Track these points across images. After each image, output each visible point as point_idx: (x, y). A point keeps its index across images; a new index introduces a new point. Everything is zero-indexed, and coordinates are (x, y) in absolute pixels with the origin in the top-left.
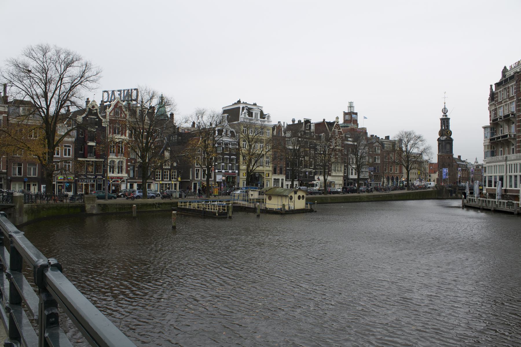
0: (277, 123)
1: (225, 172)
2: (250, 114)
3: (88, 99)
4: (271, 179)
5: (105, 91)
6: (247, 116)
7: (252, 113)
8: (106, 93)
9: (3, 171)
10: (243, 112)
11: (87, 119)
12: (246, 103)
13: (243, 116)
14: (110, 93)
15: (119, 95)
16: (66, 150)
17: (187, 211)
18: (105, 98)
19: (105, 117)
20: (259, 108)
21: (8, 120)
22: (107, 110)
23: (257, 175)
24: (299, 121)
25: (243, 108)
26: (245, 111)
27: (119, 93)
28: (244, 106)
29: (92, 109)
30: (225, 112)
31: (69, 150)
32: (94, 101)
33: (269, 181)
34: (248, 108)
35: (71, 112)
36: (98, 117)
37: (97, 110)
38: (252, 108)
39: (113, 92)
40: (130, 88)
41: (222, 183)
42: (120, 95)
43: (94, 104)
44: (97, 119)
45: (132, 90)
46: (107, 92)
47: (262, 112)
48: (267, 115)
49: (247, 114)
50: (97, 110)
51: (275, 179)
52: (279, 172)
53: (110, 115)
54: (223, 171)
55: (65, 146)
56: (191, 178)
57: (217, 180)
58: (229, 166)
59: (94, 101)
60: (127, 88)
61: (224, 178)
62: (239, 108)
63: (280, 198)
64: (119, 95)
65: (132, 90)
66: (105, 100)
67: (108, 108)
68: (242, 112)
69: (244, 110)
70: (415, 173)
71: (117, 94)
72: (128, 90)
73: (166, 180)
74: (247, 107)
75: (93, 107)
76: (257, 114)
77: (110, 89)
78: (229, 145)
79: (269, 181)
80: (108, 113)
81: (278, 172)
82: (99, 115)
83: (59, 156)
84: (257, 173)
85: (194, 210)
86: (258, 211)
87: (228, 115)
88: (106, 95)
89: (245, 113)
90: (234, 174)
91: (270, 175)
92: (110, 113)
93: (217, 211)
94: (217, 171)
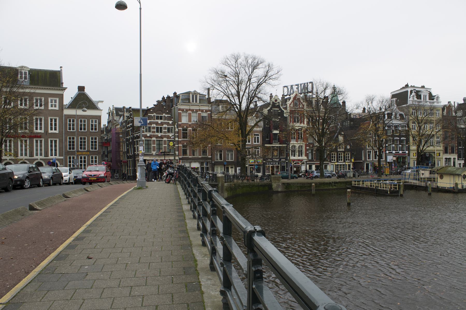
2: (419, 97)
3: (271, 94)
4: (443, 158)
5: (285, 87)
6: (416, 99)
7: (420, 96)
8: (286, 88)
10: (412, 96)
13: (411, 99)
14: (289, 87)
17: (360, 189)
18: (285, 92)
19: (286, 108)
21: (211, 116)
22: (288, 102)
23: (428, 154)
25: (411, 92)
26: (413, 94)
27: (297, 87)
28: (412, 89)
29: (275, 102)
30: (393, 96)
31: (258, 138)
32: (276, 96)
33: (440, 160)
35: (258, 107)
36: (280, 109)
37: (279, 103)
38: (420, 91)
39: (292, 86)
40: (306, 82)
41: (393, 163)
42: (298, 88)
43: (276, 98)
45: (307, 83)
46: (287, 87)
47: (430, 94)
48: (435, 96)
49: (416, 96)
50: (279, 103)
51: (446, 158)
52: (450, 151)
53: (290, 107)
54: (394, 152)
55: (255, 135)
57: (388, 161)
58: (399, 147)
59: (276, 96)
60: (304, 82)
61: (395, 159)
62: (407, 91)
63: (452, 178)
65: (307, 83)
66: (285, 94)
67: (288, 100)
68: (410, 95)
69: (413, 93)
71: (295, 88)
72: (305, 84)
73: (341, 161)
74: (415, 90)
75: (276, 100)
76: (426, 96)
77: (289, 84)
79: (440, 160)
80: (288, 105)
81: (449, 152)
82: (281, 107)
84: (427, 153)
85: (367, 189)
86: (430, 190)
87: (396, 99)
88: (286, 89)
89: (413, 96)
90: (404, 155)
91: (441, 154)
92: (290, 105)
93: (389, 189)
94: (387, 152)
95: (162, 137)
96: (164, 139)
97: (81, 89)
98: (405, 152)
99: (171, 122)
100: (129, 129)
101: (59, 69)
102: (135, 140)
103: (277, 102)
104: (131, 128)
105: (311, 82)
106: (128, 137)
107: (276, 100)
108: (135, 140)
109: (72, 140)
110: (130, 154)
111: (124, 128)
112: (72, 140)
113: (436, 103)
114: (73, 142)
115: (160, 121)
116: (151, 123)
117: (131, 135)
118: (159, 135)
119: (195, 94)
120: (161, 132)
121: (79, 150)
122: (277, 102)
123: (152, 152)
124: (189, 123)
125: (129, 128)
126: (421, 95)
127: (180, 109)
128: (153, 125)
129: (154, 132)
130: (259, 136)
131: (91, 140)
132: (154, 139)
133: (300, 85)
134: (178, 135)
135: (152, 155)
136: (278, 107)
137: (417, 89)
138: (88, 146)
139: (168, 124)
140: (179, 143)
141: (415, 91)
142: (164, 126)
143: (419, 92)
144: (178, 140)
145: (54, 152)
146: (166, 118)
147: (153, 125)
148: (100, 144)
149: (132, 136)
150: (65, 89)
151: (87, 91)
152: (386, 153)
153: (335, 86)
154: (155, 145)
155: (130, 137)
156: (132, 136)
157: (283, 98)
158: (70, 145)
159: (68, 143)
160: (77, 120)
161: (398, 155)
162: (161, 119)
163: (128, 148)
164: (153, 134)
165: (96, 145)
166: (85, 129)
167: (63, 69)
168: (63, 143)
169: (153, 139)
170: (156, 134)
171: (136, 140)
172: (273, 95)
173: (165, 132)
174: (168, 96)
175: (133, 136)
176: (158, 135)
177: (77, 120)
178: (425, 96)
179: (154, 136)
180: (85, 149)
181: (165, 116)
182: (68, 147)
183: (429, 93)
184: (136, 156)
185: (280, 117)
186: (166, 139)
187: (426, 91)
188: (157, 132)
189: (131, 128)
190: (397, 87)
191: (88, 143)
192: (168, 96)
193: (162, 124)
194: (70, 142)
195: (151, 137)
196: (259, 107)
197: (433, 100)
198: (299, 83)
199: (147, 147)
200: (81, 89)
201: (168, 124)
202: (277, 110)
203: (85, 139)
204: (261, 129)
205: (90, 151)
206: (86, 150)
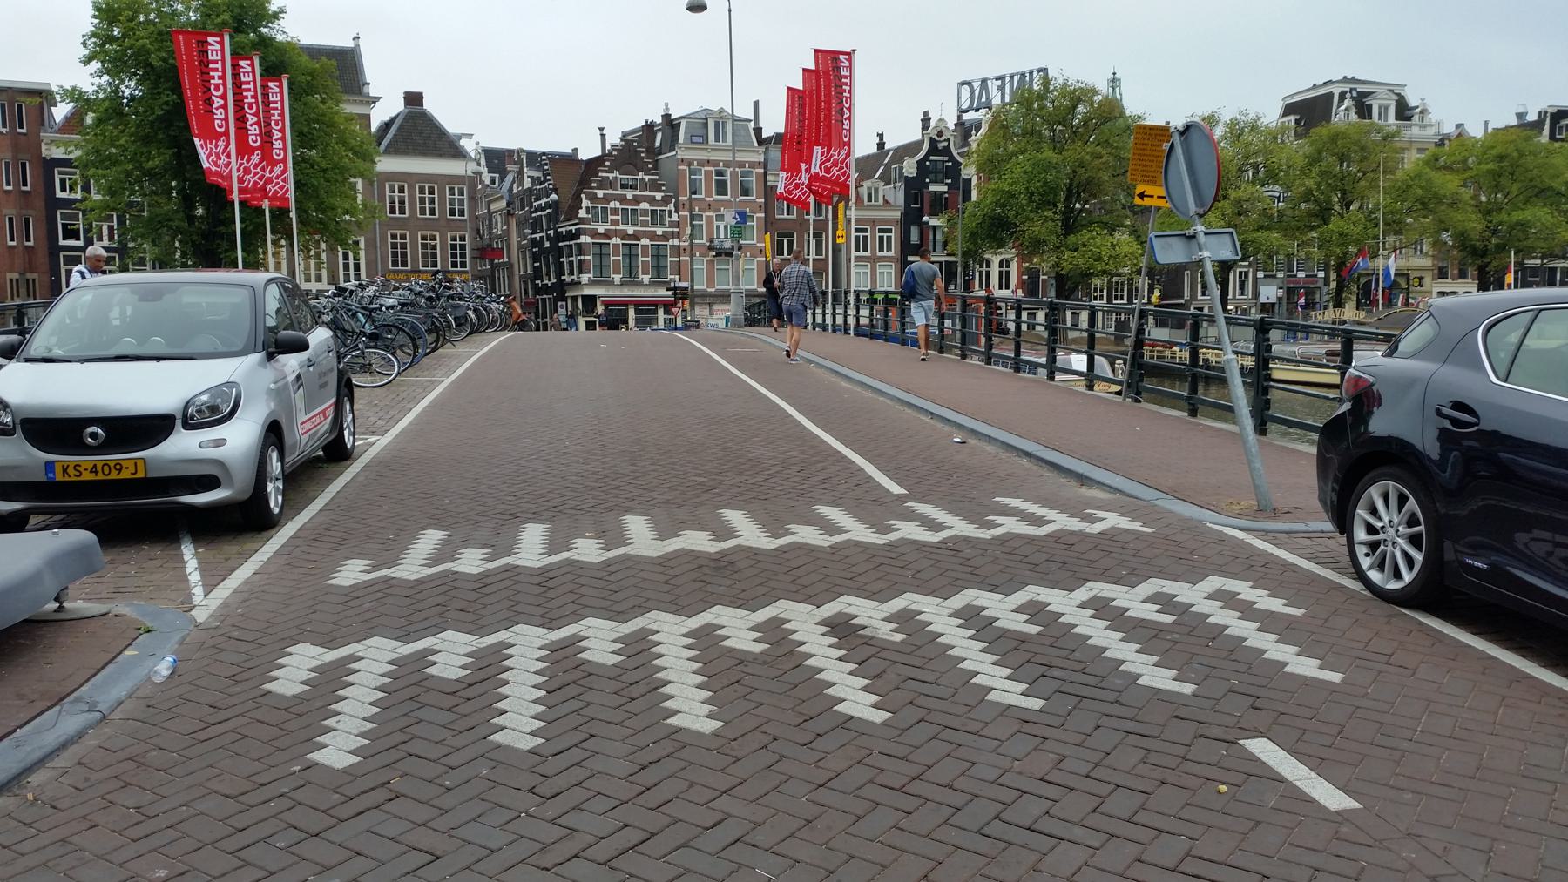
0: (1449, 129)
1: (1307, 276)
2: (1364, 110)
3: (926, 113)
5: (963, 83)
6: (1353, 117)
8: (966, 87)
9: (709, 290)
10: (1343, 108)
11: (928, 163)
12: (1353, 80)
13: (1343, 116)
14: (976, 85)
15: (998, 88)
16: (881, 238)
18: (963, 100)
20: (1392, 91)
22: (973, 137)
24: (1540, 113)
25: (1342, 96)
26: (1347, 103)
27: (999, 83)
28: (1346, 87)
29: (937, 138)
30: (1289, 110)
31: (889, 238)
32: (941, 120)
34: (1358, 93)
35: (889, 151)
36: (952, 158)
37: (948, 140)
38: (1371, 93)
39: (984, 81)
40: (1025, 68)
42: (1001, 88)
43: (941, 127)
44: (948, 161)
45: (1031, 73)
46: (969, 83)
48: (1417, 107)
49: (1354, 110)
50: (948, 140)
52: (1456, 272)
54: (1280, 275)
55: (881, 231)
56: (1187, 295)
57: (1263, 299)
59: (941, 120)
60: (1021, 70)
62: (1331, 95)
64: (998, 88)
65: (1031, 73)
66: (965, 107)
67: (974, 132)
68: (1339, 107)
70: (631, 254)
71: (993, 87)
72: (1023, 75)
73: (1119, 302)
74: (1355, 89)
75: (940, 134)
76: (1386, 108)
77: (975, 76)
78: (1279, 201)
80: (974, 146)
82: (955, 153)
83: (868, 254)
87: (1298, 117)
88: (966, 90)
89: (1347, 109)
90: (1312, 283)
91: (1427, 281)
94: (1260, 274)
95: (636, 236)
96: (643, 242)
97: (414, 99)
98: (1316, 276)
99: (659, 196)
100: (539, 213)
101: (350, 44)
102: (560, 244)
103: (943, 138)
104: (548, 211)
105: (1045, 70)
106: (538, 236)
107: (940, 134)
108: (560, 244)
109: (399, 241)
110: (546, 282)
111: (523, 209)
112: (399, 241)
113: (1418, 128)
114: (404, 246)
115: (630, 194)
116: (607, 199)
117: (547, 231)
118: (630, 230)
119: (722, 118)
120: (605, 221)
121: (450, 269)
122: (943, 138)
123: (641, 276)
124: (707, 199)
125: (540, 208)
126: (1370, 106)
127: (682, 160)
128: (612, 205)
129: (615, 222)
130: (893, 235)
131: (449, 242)
132: (616, 240)
133: (1007, 79)
134: (678, 232)
135: (640, 284)
136: (947, 151)
137: (1362, 88)
138: (415, 260)
139: (652, 201)
140: (682, 251)
141: (1355, 94)
142: (642, 206)
143: (1365, 97)
144: (679, 246)
145: (352, 272)
146: (644, 185)
147: (612, 205)
148: (476, 254)
149: (551, 232)
150: (375, 100)
151: (429, 105)
152: (1256, 279)
153: (1117, 76)
154: (649, 259)
155: (544, 234)
156: (551, 232)
157: (960, 123)
158: (395, 255)
159: (390, 250)
160: (412, 188)
161: (1293, 282)
162: (633, 187)
163: (536, 264)
164: (613, 228)
165: (463, 256)
166: (402, 211)
167: (361, 42)
168: (376, 248)
169: (614, 240)
170: (622, 227)
171: (567, 243)
172: (930, 115)
173: (644, 224)
174: (575, 150)
175: (556, 232)
176: (626, 231)
177: (412, 188)
178: (1384, 110)
179: (616, 233)
180: (404, 264)
181: (643, 180)
182: (390, 259)
183: (1397, 98)
184: (566, 288)
185: (950, 181)
186: (648, 242)
187: (1390, 94)
188: (654, 223)
189: (548, 211)
190: (1302, 81)
191: (443, 250)
192: (575, 150)
193: (636, 200)
194: (394, 246)
195: (607, 235)
196: (891, 153)
197: (1409, 119)
198: (1007, 71)
199: (598, 263)
200: (414, 99)
201: (652, 201)
202: (944, 162)
203: (403, 237)
204: (897, 214)
205: (420, 271)
206: (409, 268)
